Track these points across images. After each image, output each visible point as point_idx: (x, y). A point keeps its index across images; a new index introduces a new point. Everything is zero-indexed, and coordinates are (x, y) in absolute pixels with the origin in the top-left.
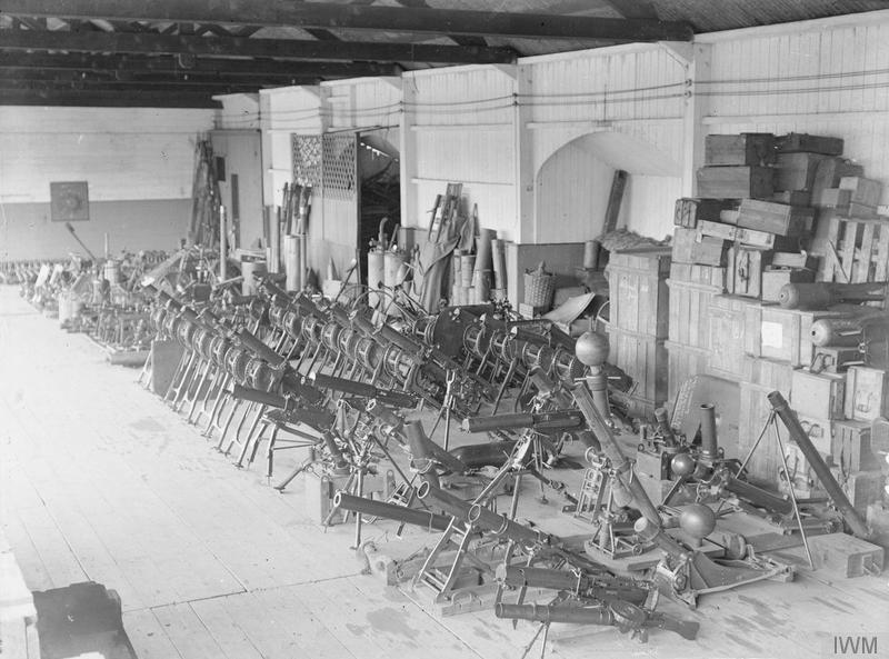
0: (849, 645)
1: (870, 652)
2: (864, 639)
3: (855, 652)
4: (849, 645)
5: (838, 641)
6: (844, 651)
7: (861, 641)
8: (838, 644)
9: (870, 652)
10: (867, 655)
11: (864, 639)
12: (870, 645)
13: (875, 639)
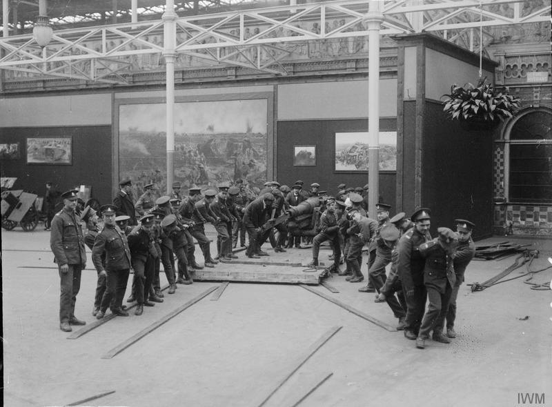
0: (527, 399)
1: (540, 403)
3: (531, 402)
4: (527, 399)
5: (521, 397)
6: (524, 403)
7: (535, 396)
8: (521, 397)
10: (538, 405)
11: (537, 395)
12: (540, 399)
13: (543, 395)
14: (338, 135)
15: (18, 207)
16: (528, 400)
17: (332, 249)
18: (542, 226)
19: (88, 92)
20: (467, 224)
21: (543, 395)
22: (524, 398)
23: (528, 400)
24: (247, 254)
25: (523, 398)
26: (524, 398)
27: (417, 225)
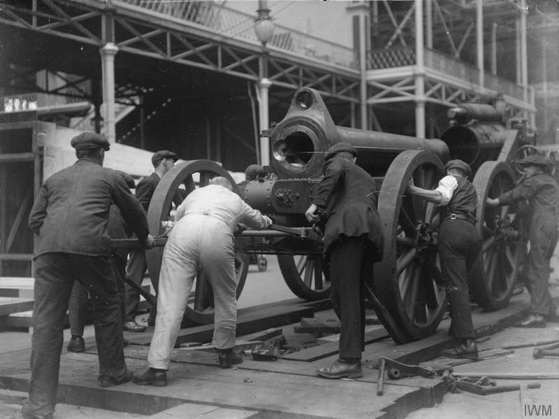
0: (534, 410)
1: (547, 414)
2: (543, 406)
4: (534, 410)
6: (531, 414)
7: (541, 408)
9: (547, 414)
10: (545, 416)
11: (543, 406)
13: (550, 407)
22: (531, 409)
26: (531, 409)
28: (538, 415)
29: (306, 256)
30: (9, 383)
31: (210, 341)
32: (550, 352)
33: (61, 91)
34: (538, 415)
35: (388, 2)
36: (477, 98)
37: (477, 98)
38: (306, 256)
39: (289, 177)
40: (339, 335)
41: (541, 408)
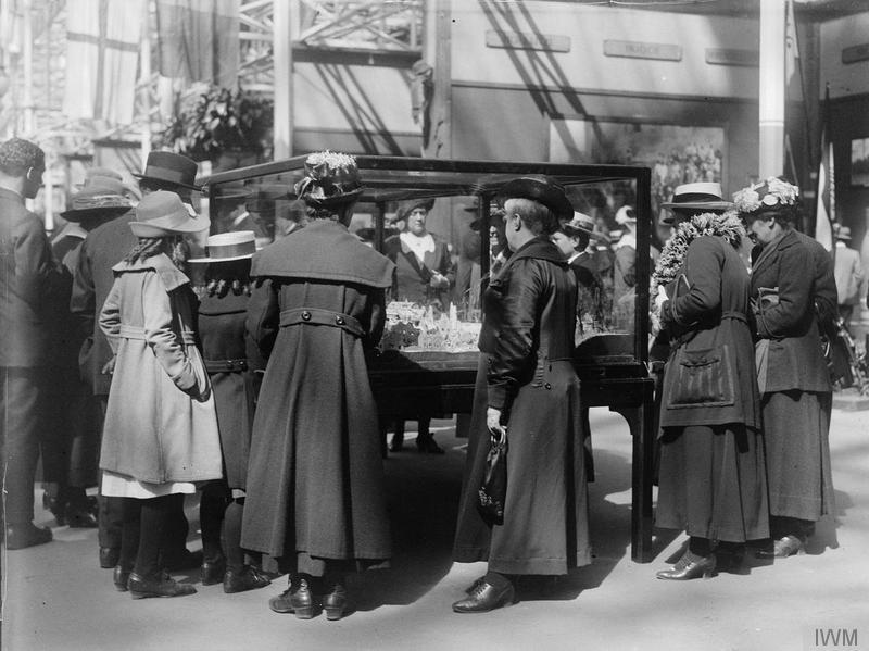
0: (830, 637)
1: (850, 644)
2: (845, 631)
4: (830, 637)
6: (825, 644)
7: (841, 634)
9: (850, 644)
10: (847, 647)
11: (845, 631)
12: (851, 637)
13: (855, 631)
14: (202, 547)
15: (726, 555)
16: (830, 641)
17: (26, 377)
18: (690, 364)
19: (290, 465)
20: (775, 216)
21: (855, 631)
22: (825, 636)
23: (830, 641)
24: (634, 557)
25: (823, 636)
26: (825, 636)
27: (127, 119)
28: (836, 644)
29: (95, 393)
30: (103, 11)
31: (153, 69)
32: (373, 118)
33: (335, 73)
34: (836, 644)
35: (794, 2)
36: (681, 182)
37: (681, 182)
38: (95, 393)
39: (830, 182)
40: (287, 576)
41: (841, 634)
